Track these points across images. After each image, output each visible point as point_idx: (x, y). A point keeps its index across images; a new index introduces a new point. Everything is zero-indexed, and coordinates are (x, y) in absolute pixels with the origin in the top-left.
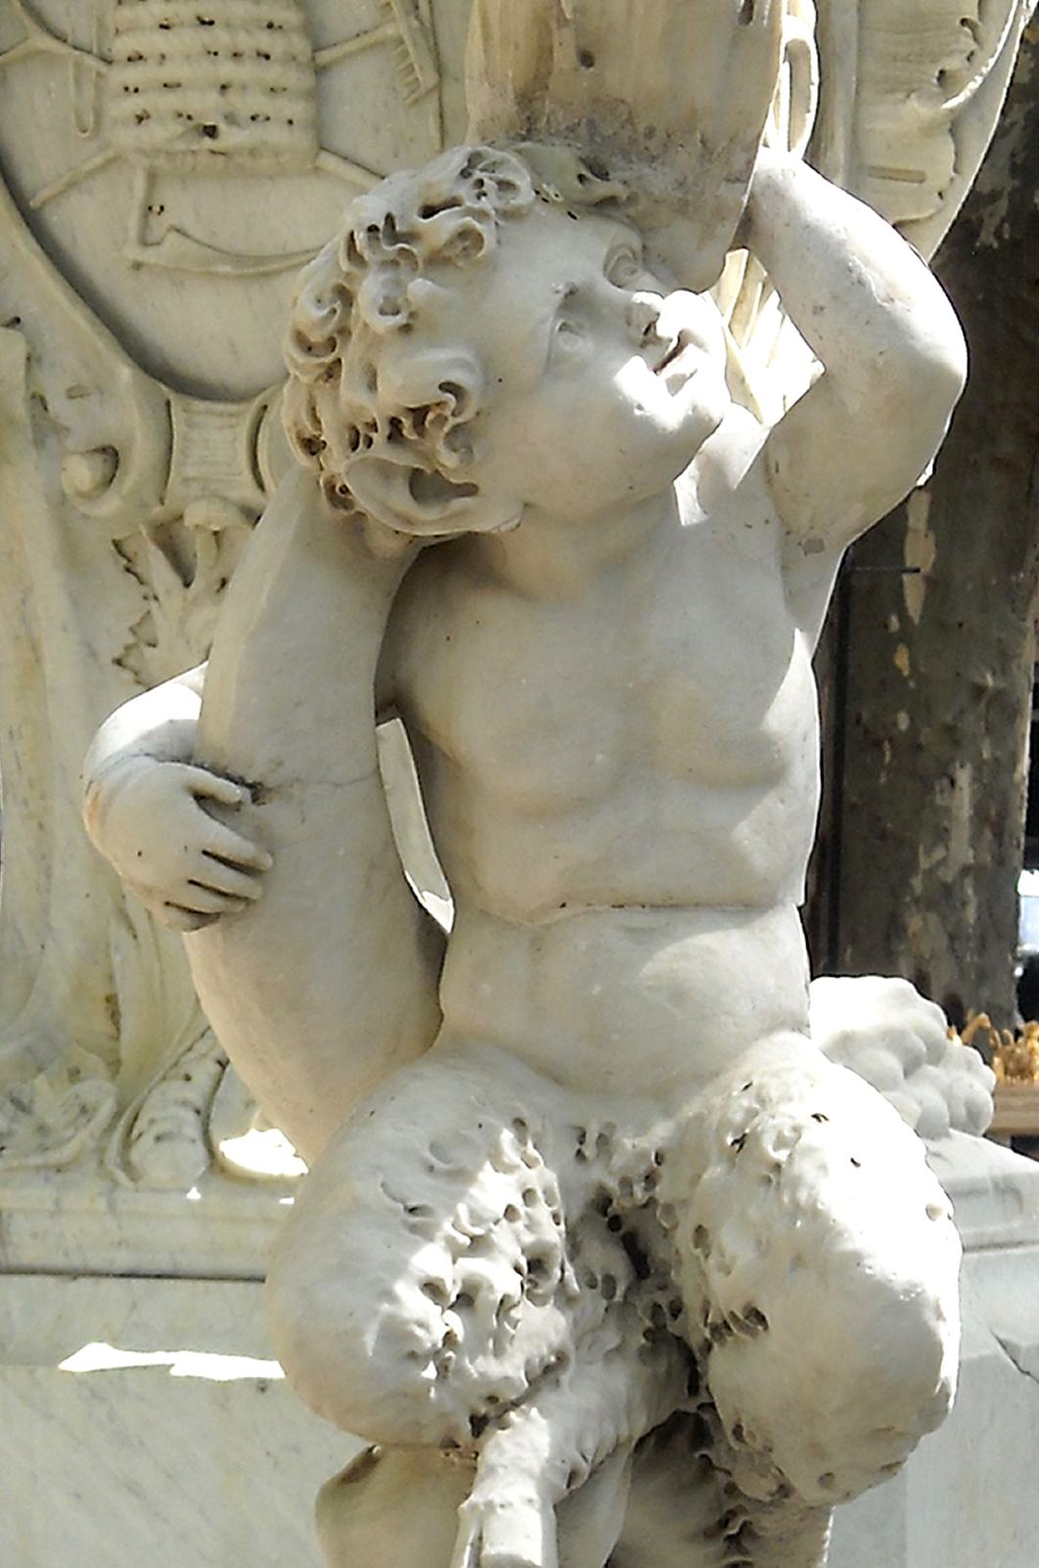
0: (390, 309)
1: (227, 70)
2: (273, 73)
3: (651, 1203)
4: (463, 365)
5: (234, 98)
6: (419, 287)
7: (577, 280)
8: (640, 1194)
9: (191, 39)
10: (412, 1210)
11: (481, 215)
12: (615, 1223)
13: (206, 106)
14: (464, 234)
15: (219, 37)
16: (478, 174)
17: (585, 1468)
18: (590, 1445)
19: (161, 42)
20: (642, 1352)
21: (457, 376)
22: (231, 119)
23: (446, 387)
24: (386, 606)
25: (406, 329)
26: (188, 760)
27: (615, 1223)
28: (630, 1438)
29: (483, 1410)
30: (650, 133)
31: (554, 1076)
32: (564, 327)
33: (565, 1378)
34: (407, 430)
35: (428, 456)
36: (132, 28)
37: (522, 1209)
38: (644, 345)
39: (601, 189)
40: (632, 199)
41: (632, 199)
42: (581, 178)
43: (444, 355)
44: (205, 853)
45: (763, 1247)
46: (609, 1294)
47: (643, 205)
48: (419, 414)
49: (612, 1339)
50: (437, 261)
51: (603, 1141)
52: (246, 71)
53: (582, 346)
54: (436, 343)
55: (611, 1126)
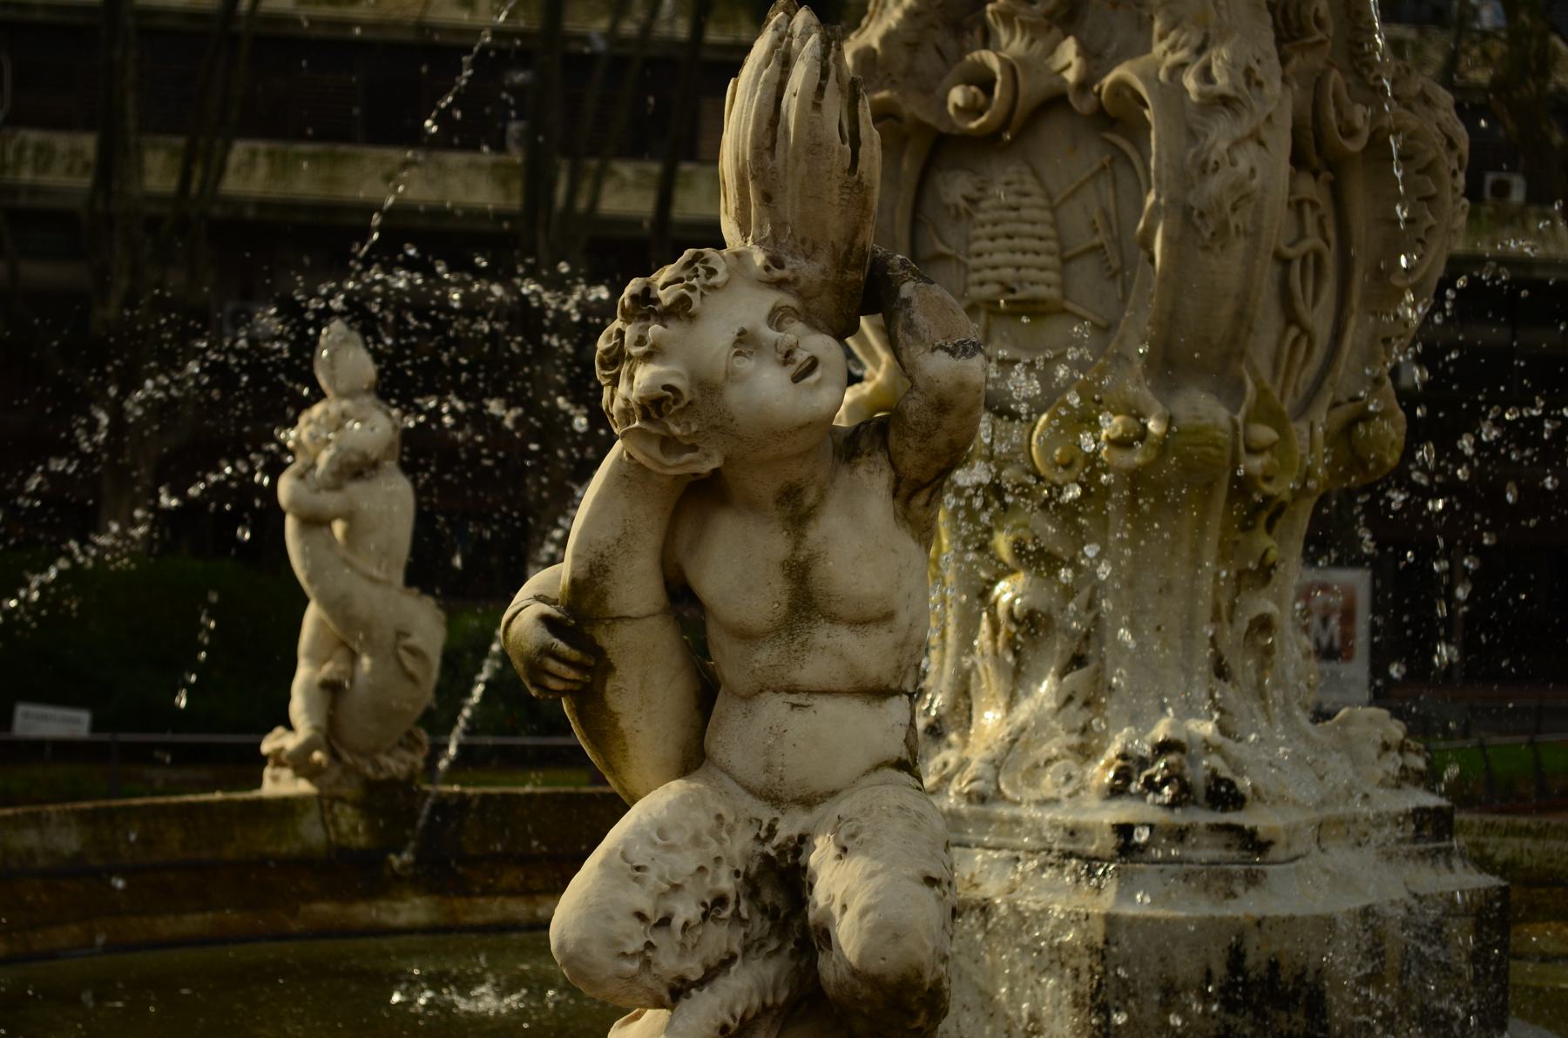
0: (640, 341)
1: (1019, 258)
2: (1043, 260)
4: (679, 375)
5: (1023, 272)
6: (655, 329)
7: (746, 326)
9: (1002, 242)
10: (638, 868)
11: (692, 288)
13: (1008, 274)
15: (1016, 242)
16: (697, 265)
17: (734, 1025)
18: (739, 1010)
19: (987, 245)
22: (1020, 282)
23: (666, 387)
32: (737, 354)
33: (733, 969)
34: (654, 415)
35: (666, 428)
36: (978, 238)
39: (777, 274)
50: (666, 315)
52: (1030, 258)
53: (746, 365)
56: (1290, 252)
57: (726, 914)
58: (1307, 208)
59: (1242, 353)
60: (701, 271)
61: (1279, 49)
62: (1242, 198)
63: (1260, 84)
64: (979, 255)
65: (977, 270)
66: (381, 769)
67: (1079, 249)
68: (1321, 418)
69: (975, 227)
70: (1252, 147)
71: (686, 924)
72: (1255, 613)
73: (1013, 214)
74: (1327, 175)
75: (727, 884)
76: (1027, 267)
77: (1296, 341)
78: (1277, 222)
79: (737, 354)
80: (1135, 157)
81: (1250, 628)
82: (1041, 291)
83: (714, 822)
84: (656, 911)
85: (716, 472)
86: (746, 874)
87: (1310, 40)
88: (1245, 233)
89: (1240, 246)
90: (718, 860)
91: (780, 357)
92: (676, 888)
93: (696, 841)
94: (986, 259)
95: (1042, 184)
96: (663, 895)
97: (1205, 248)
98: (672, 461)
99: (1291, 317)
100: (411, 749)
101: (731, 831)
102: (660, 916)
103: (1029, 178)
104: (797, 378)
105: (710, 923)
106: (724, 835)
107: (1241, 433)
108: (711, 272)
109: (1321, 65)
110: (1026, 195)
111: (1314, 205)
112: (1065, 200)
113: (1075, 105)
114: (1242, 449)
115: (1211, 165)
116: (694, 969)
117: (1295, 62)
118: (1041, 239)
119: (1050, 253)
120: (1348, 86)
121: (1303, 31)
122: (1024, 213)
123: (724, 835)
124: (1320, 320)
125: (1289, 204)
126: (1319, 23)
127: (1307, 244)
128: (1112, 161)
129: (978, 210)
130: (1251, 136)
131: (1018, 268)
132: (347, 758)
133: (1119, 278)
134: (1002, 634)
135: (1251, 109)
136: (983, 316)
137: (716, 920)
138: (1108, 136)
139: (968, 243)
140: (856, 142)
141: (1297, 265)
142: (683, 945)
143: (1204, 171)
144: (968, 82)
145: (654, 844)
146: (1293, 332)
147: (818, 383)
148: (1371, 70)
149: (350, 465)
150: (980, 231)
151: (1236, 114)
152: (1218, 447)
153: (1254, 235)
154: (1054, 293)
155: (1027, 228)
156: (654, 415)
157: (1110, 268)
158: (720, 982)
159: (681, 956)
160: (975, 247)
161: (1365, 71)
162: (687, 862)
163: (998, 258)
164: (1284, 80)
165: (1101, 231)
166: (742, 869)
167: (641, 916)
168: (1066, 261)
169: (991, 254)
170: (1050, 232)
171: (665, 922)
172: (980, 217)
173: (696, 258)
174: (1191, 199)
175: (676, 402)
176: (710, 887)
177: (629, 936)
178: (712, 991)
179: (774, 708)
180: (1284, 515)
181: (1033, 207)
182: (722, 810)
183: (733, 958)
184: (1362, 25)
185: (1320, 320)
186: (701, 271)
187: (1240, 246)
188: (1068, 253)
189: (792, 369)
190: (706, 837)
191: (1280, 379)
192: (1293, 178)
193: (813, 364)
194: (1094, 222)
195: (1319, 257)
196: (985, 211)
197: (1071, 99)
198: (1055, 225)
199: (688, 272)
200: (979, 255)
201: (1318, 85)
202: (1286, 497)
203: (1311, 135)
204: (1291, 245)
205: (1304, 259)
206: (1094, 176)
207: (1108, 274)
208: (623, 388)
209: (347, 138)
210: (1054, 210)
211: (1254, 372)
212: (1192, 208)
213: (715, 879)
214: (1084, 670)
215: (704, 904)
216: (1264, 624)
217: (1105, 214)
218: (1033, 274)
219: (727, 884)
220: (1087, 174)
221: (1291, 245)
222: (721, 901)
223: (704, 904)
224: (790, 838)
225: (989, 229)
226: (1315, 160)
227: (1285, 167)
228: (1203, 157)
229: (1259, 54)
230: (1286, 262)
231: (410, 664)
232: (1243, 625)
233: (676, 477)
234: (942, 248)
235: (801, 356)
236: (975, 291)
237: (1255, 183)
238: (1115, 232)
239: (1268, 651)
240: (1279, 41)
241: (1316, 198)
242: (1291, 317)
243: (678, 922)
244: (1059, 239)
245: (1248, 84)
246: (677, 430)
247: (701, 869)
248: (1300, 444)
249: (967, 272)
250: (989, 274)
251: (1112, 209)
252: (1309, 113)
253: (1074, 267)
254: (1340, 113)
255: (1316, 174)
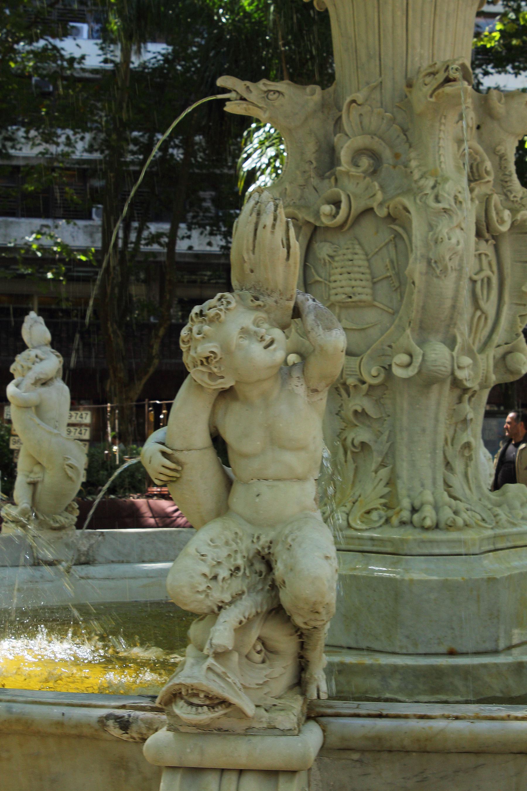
1: (353, 283)
2: (364, 283)
3: (270, 553)
4: (216, 347)
7: (244, 326)
8: (266, 551)
9: (346, 276)
10: (203, 555)
11: (221, 310)
12: (263, 558)
13: (348, 290)
14: (217, 314)
15: (352, 276)
16: (223, 300)
18: (247, 615)
19: (339, 277)
20: (268, 591)
21: (213, 350)
22: (354, 294)
24: (210, 406)
25: (203, 338)
26: (163, 444)
27: (263, 558)
28: (262, 612)
29: (220, 604)
30: (267, 289)
31: (250, 522)
33: (244, 597)
34: (205, 363)
35: (210, 369)
36: (334, 274)
37: (233, 555)
38: (261, 341)
40: (265, 306)
41: (265, 306)
42: (252, 301)
43: (210, 345)
44: (163, 466)
45: (286, 566)
46: (260, 575)
47: (267, 307)
48: (207, 358)
49: (260, 587)
50: (211, 321)
51: (258, 538)
52: (358, 283)
54: (210, 342)
55: (260, 534)
56: (475, 277)
57: (240, 574)
58: (483, 257)
59: (455, 324)
60: (225, 303)
61: (469, 185)
62: (454, 254)
63: (461, 202)
64: (335, 281)
65: (334, 288)
66: (57, 522)
67: (380, 278)
68: (492, 353)
69: (333, 269)
70: (458, 231)
71: (224, 578)
72: (465, 440)
73: (350, 263)
74: (492, 242)
75: (240, 562)
76: (357, 287)
77: (480, 317)
78: (471, 266)
79: (241, 337)
80: (405, 236)
81: (461, 448)
82: (364, 297)
83: (234, 536)
84: (211, 573)
85: (232, 388)
86: (248, 557)
87: (483, 181)
88: (455, 270)
89: (453, 276)
90: (236, 552)
91: (259, 339)
92: (219, 563)
93: (227, 543)
94: (338, 284)
95: (363, 248)
96: (214, 566)
97: (438, 277)
98: (212, 383)
99: (476, 306)
100: (71, 513)
101: (241, 539)
102: (213, 575)
103: (357, 247)
104: (266, 347)
105: (233, 578)
106: (239, 541)
107: (455, 361)
108: (229, 303)
109: (489, 192)
110: (356, 254)
111: (486, 255)
112: (373, 256)
113: (377, 213)
114: (456, 367)
115: (440, 240)
116: (227, 598)
117: (476, 192)
118: (363, 274)
119: (367, 280)
120: (501, 201)
121: (481, 177)
122: (355, 262)
123: (239, 541)
124: (490, 307)
125: (475, 256)
126: (487, 173)
127: (483, 275)
128: (394, 238)
129: (334, 261)
130: (457, 226)
131: (353, 287)
132: (41, 517)
133: (399, 290)
134: (349, 453)
135: (457, 214)
136: (337, 310)
137: (236, 577)
138: (392, 226)
139: (330, 276)
140: (289, 247)
141: (479, 285)
142: (223, 588)
143: (436, 243)
144: (329, 203)
145: (209, 545)
146: (478, 313)
147: (275, 350)
148: (511, 193)
149: (40, 379)
150: (336, 271)
151: (450, 216)
152: (445, 367)
153: (460, 270)
154: (369, 298)
155: (356, 269)
156: (205, 363)
157: (394, 286)
158: (239, 603)
159: (222, 591)
160: (333, 278)
161: (509, 193)
162: (224, 552)
163: (344, 283)
164: (472, 200)
165: (390, 270)
166: (246, 555)
167: (205, 575)
168: (374, 283)
169: (340, 281)
170: (367, 271)
171: (215, 578)
172: (335, 264)
173: (222, 297)
174: (431, 255)
175: (215, 358)
176: (233, 563)
177: (200, 584)
178: (235, 606)
179: (263, 487)
180: (476, 396)
181: (360, 260)
182: (238, 531)
183: (243, 593)
184: (507, 173)
185: (490, 307)
186: (225, 303)
187: (453, 276)
188: (375, 280)
189: (264, 343)
190: (231, 542)
191: (473, 335)
192: (477, 243)
193: (272, 342)
194: (387, 266)
195: (489, 279)
196: (337, 262)
197: (376, 210)
198: (369, 267)
199: (219, 303)
200: (335, 281)
201: (487, 201)
202: (477, 388)
203: (484, 224)
204: (476, 274)
205: (482, 280)
206: (387, 244)
207: (394, 289)
208: (192, 353)
209: (13, 214)
210: (368, 260)
211: (462, 334)
212: (431, 259)
213: (235, 560)
214: (386, 469)
215: (231, 570)
216: (468, 446)
217: (392, 262)
218: (360, 290)
219: (240, 562)
220: (383, 244)
221: (476, 274)
222: (238, 569)
223: (231, 570)
224: (266, 542)
225: (339, 270)
226: (487, 236)
227: (473, 238)
228: (436, 236)
229: (460, 189)
230: (474, 282)
231: (70, 472)
232: (458, 447)
233: (215, 390)
234: (318, 278)
235: (268, 338)
236: (333, 298)
237: (460, 247)
238: (397, 269)
239: (470, 458)
240: (470, 181)
241: (487, 252)
242: (476, 306)
243: (220, 578)
244: (371, 273)
245: (456, 203)
246: (215, 370)
247: (229, 556)
248: (482, 364)
249: (330, 289)
250: (340, 290)
251: (394, 257)
252: (483, 214)
253: (378, 286)
254: (497, 214)
255: (487, 241)
